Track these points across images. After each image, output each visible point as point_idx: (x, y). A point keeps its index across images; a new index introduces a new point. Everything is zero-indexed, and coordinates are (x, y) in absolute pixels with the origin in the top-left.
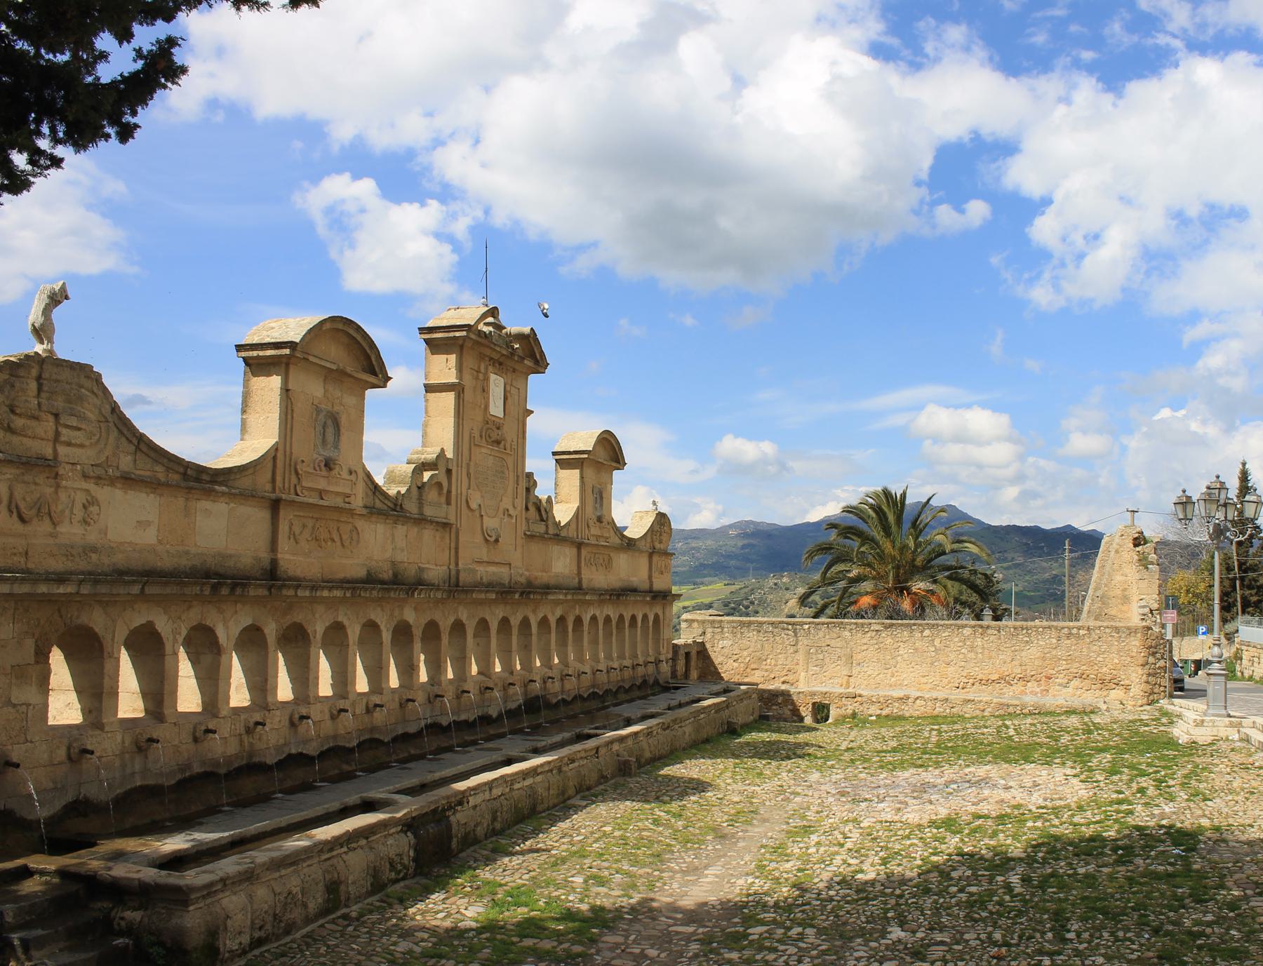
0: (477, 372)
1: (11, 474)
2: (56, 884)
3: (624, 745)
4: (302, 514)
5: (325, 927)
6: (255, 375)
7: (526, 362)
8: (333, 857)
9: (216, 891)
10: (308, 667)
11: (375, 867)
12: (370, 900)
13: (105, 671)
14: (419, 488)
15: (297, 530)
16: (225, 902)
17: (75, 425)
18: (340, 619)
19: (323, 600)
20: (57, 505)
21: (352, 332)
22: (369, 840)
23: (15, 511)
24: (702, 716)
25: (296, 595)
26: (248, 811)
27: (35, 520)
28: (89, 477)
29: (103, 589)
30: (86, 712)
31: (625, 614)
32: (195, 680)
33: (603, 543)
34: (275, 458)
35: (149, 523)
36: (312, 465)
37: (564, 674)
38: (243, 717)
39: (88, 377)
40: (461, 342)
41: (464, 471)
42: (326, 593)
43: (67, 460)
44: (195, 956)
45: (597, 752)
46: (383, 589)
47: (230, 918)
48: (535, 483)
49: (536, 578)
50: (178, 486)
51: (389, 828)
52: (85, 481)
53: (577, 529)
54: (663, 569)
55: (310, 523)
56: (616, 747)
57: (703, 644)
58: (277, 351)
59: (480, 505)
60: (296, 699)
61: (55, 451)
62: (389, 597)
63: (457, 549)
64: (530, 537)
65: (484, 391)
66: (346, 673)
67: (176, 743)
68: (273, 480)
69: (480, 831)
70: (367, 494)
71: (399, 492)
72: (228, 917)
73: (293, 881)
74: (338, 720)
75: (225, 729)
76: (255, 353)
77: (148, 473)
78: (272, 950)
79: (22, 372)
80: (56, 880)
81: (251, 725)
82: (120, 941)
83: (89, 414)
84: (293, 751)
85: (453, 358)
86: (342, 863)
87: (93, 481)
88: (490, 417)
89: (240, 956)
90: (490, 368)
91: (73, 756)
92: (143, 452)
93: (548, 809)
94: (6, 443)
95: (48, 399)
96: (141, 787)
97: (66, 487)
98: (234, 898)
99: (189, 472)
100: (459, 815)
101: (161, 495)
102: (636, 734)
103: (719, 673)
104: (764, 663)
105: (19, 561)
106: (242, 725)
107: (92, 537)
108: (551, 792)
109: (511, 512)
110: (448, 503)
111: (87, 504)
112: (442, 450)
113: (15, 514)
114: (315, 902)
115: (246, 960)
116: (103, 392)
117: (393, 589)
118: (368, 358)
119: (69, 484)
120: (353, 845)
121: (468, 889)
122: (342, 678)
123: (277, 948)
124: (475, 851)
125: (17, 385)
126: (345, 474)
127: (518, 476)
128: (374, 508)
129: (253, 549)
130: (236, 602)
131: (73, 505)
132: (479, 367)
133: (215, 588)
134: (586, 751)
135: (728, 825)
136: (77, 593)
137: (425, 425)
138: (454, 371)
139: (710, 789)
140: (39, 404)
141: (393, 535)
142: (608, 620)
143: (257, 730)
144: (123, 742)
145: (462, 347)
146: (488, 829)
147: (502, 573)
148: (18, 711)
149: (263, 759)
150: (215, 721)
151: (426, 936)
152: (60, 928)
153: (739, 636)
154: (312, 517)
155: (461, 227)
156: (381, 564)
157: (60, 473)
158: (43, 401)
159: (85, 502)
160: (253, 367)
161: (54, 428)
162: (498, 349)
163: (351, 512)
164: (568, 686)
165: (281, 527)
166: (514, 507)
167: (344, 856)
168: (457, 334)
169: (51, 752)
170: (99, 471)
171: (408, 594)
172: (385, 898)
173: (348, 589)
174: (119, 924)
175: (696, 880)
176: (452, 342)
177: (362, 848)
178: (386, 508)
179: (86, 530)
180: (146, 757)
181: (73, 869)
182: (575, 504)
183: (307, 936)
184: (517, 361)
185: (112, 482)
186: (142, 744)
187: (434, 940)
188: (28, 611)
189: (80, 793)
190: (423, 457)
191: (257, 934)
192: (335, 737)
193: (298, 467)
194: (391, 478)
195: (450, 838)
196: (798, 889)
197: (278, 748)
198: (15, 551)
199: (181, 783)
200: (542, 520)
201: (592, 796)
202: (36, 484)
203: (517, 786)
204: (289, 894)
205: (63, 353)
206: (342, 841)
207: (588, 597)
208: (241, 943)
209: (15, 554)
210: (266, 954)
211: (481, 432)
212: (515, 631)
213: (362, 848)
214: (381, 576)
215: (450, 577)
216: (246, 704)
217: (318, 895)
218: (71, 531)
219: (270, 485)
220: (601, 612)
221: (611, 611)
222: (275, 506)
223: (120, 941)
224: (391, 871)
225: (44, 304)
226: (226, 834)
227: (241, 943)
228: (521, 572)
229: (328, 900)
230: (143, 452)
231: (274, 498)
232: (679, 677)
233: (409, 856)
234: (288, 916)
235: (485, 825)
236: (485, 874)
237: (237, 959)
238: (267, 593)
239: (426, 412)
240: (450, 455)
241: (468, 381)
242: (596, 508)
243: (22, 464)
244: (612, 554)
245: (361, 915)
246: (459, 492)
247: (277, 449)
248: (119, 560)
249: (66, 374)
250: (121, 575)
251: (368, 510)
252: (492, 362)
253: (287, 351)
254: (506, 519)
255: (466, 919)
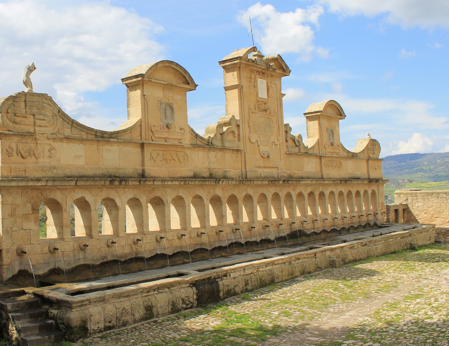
0: (250, 78)
1: (16, 140)
2: (32, 298)
3: (333, 253)
4: (156, 149)
5: (144, 325)
6: (131, 91)
7: (277, 71)
8: (149, 295)
9: (85, 304)
10: (165, 216)
11: (173, 302)
12: (170, 316)
13: (64, 217)
14: (221, 134)
15: (154, 156)
16: (90, 310)
17: (42, 118)
18: (180, 195)
19: (169, 186)
20: (37, 151)
21: (174, 67)
22: (170, 289)
23: (19, 154)
24: (391, 240)
25: (154, 184)
26: (125, 275)
27: (28, 158)
28: (50, 139)
29: (57, 183)
30: (59, 233)
31: (352, 190)
32: (110, 222)
33: (334, 156)
34: (141, 125)
35: (80, 156)
36: (159, 127)
37: (314, 220)
38: (131, 237)
39: (46, 99)
40: (238, 65)
41: (247, 125)
42: (170, 183)
43: (40, 132)
44: (76, 330)
45: (315, 256)
46: (201, 180)
47: (93, 316)
48: (290, 129)
49: (295, 174)
50: (92, 140)
51: (182, 284)
52: (49, 140)
53: (319, 150)
54: (376, 168)
55: (161, 153)
56: (328, 253)
57: (407, 205)
58: (136, 79)
59: (257, 141)
60: (161, 230)
61: (35, 129)
62: (205, 184)
63: (245, 161)
64: (290, 154)
65: (255, 87)
66: (186, 219)
67: (99, 247)
68: (141, 135)
69: (237, 289)
70: (192, 139)
71: (210, 137)
72: (91, 315)
73: (126, 304)
74: (182, 239)
75: (123, 242)
76: (128, 82)
77: (78, 136)
78: (115, 332)
79: (18, 100)
80: (33, 296)
81: (135, 240)
82: (50, 321)
83: (48, 114)
84: (159, 252)
85: (235, 73)
86: (154, 298)
87: (52, 140)
88: (259, 99)
89: (99, 332)
90: (257, 76)
91: (51, 250)
92: (75, 127)
93: (282, 281)
94: (14, 128)
95: (30, 109)
96: (83, 264)
97: (40, 143)
98: (95, 308)
99: (98, 134)
100: (224, 281)
101: (85, 144)
102: (342, 247)
103: (417, 220)
104: (442, 214)
105: (22, 174)
106: (131, 240)
107: (54, 163)
108: (284, 273)
109: (277, 143)
110: (239, 140)
111: (50, 150)
112: (233, 116)
113: (20, 155)
114: (140, 313)
115: (102, 334)
116: (53, 104)
117: (206, 180)
118: (185, 77)
119: (41, 142)
120: (160, 291)
121: (220, 314)
122: (185, 220)
123: (118, 331)
124: (234, 298)
125: (16, 105)
126: (178, 130)
127: (279, 126)
128: (196, 144)
129: (133, 165)
130: (125, 188)
131: (44, 151)
132: (251, 76)
133: (111, 182)
134: (307, 254)
135: (375, 292)
136: (46, 185)
137: (227, 106)
138: (236, 79)
139: (377, 275)
140: (26, 111)
141: (208, 156)
142: (341, 193)
143: (139, 243)
144: (74, 246)
145: (239, 68)
146: (243, 289)
147: (274, 173)
148: (26, 232)
149: (143, 256)
150: (117, 238)
151: (185, 332)
152: (27, 314)
153: (427, 200)
154: (162, 150)
155: (314, 17)
156: (202, 169)
157: (37, 138)
158: (28, 110)
159: (49, 149)
160: (130, 88)
161: (33, 120)
162: (259, 66)
163: (183, 147)
164: (317, 226)
165: (145, 155)
166: (278, 140)
167: (156, 295)
168: (236, 62)
169: (42, 248)
170: (54, 136)
171: (216, 182)
172: (178, 316)
173: (182, 181)
174: (50, 315)
175: (338, 317)
176: (235, 66)
177: (166, 292)
178: (203, 144)
179: (51, 160)
180: (85, 252)
181: (37, 293)
182: (316, 138)
183: (134, 328)
184: (272, 71)
185: (61, 140)
186: (82, 247)
187: (188, 334)
188: (27, 193)
189: (56, 266)
190: (224, 120)
191: (108, 324)
192: (181, 247)
193: (152, 128)
194: (208, 131)
195: (219, 291)
196: (387, 324)
197: (150, 251)
198: (20, 170)
199: (102, 264)
200: (297, 146)
201: (310, 276)
202: (27, 143)
203: (261, 269)
204: (124, 309)
205: (35, 91)
206: (154, 288)
207: (325, 182)
208: (99, 327)
209: (20, 171)
210: (112, 333)
211: (255, 106)
212: (283, 199)
213: (166, 292)
214: (202, 175)
215: (242, 175)
216: (136, 232)
217: (141, 311)
218: (44, 161)
219: (140, 137)
220: (336, 190)
221: (344, 189)
222: (142, 145)
223: (50, 321)
224: (182, 304)
225: (26, 72)
226: (105, 283)
227: (99, 327)
228: (284, 171)
229: (146, 314)
230: (75, 127)
231: (141, 143)
232: (391, 222)
233: (194, 298)
234: (123, 318)
235: (241, 287)
236: (232, 308)
237: (97, 334)
238: (139, 184)
239: (226, 100)
240: (237, 118)
241: (245, 83)
242: (330, 139)
243: (20, 135)
244: (341, 161)
245: (163, 321)
246: (244, 135)
247: (141, 121)
248: (68, 172)
249: (36, 99)
250: (69, 178)
251: (193, 146)
252: (258, 73)
253: (140, 78)
254: (274, 146)
255: (209, 326)
